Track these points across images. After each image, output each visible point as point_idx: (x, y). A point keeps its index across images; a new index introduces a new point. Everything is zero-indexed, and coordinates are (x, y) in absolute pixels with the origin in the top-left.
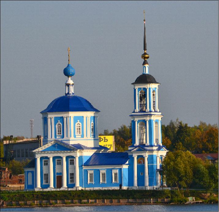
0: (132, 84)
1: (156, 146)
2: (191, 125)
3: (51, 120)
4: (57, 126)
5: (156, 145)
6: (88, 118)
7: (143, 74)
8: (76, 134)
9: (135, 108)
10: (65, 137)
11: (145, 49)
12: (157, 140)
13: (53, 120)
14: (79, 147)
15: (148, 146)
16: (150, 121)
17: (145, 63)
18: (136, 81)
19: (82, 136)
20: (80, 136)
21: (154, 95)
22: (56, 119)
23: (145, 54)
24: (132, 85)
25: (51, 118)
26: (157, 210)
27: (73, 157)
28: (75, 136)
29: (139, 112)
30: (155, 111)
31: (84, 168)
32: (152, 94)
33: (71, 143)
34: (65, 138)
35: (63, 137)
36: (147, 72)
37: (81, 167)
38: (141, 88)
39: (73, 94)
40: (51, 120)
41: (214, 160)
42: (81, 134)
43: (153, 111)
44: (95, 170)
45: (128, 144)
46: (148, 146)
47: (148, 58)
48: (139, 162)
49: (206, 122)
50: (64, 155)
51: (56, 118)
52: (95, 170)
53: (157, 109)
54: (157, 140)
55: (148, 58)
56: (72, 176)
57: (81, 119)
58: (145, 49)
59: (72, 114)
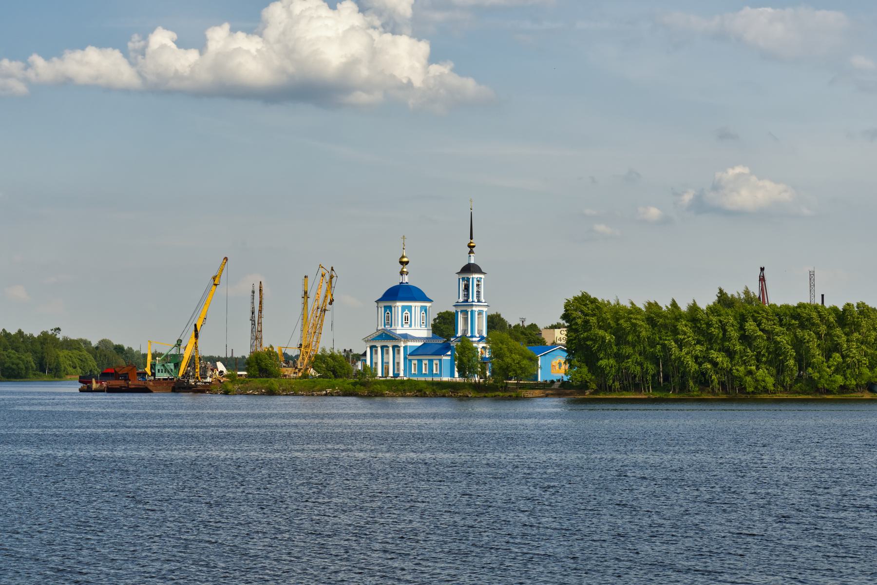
4: (386, 315)
5: (478, 335)
8: (404, 323)
11: (471, 238)
12: (480, 332)
14: (406, 337)
16: (472, 311)
17: (471, 252)
19: (411, 326)
22: (404, 308)
23: (471, 243)
24: (457, 275)
26: (46, 379)
27: (387, 347)
28: (402, 326)
30: (479, 301)
31: (410, 358)
33: (398, 332)
34: (393, 327)
35: (391, 326)
36: (472, 262)
37: (405, 358)
39: (407, 283)
42: (409, 323)
43: (476, 301)
44: (429, 360)
47: (474, 246)
49: (836, 305)
50: (390, 344)
51: (385, 307)
52: (429, 360)
53: (482, 299)
54: (480, 332)
55: (474, 246)
56: (396, 364)
57: (410, 308)
58: (471, 238)
59: (400, 304)
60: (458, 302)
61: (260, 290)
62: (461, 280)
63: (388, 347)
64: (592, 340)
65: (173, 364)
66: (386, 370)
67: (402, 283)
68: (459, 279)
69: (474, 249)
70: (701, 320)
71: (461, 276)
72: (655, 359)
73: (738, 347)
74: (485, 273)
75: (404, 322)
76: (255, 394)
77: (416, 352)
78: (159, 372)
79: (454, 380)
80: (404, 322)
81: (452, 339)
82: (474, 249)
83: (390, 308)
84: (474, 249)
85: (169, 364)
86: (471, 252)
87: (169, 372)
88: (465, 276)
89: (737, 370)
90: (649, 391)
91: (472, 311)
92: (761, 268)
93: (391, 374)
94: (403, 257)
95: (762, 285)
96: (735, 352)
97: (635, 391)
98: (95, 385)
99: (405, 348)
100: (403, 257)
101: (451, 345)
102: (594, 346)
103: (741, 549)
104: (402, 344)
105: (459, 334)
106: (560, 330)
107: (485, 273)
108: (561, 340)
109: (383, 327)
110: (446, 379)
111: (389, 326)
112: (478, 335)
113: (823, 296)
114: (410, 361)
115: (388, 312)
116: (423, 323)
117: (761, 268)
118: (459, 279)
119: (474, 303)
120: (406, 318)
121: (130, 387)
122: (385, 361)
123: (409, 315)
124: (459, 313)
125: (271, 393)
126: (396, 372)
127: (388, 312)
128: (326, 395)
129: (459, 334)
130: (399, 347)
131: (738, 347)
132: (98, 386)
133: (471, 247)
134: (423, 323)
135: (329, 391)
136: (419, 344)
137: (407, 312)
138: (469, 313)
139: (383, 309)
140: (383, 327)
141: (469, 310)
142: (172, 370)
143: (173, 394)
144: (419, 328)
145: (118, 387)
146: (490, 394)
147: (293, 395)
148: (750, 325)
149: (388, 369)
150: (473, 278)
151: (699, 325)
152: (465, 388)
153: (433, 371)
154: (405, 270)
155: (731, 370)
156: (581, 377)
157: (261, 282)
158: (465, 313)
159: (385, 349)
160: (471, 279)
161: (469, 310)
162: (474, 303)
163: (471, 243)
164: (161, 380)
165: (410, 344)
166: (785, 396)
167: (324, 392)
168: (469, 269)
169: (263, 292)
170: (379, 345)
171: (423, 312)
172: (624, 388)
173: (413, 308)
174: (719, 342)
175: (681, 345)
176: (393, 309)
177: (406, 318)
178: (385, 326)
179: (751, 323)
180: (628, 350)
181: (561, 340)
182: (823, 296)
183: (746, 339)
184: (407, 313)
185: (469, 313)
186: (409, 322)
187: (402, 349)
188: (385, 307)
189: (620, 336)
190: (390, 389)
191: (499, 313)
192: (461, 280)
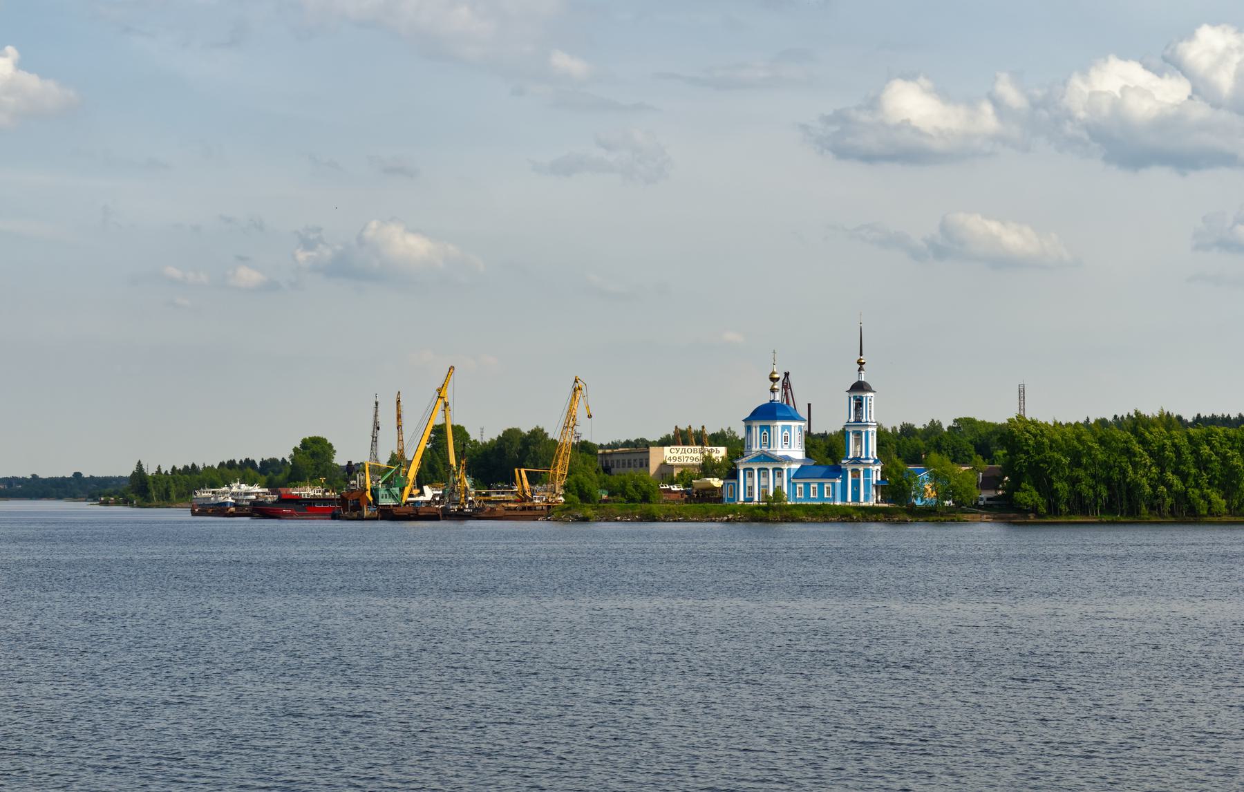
4: (762, 435)
5: (872, 458)
11: (861, 355)
16: (867, 433)
19: (790, 447)
28: (782, 447)
31: (793, 481)
33: (779, 454)
34: (772, 448)
35: (769, 447)
36: (863, 380)
37: (789, 481)
42: (768, 444)
44: (819, 484)
47: (864, 363)
50: (770, 467)
52: (819, 484)
55: (864, 363)
57: (789, 428)
58: (861, 355)
59: (780, 424)
62: (852, 398)
63: (753, 470)
64: (1046, 462)
65: (398, 489)
67: (773, 401)
68: (850, 398)
70: (1152, 443)
71: (852, 395)
72: (1108, 482)
73: (1193, 471)
74: (874, 392)
76: (628, 521)
77: (799, 474)
78: (382, 497)
79: (847, 504)
81: (843, 462)
82: (864, 366)
83: (768, 428)
85: (394, 489)
86: (860, 369)
87: (393, 497)
88: (858, 394)
89: (1193, 492)
90: (1097, 514)
92: (785, 373)
94: (774, 373)
95: (786, 394)
96: (1189, 474)
97: (1081, 514)
98: (366, 513)
99: (789, 470)
100: (774, 373)
101: (843, 467)
102: (1049, 469)
104: (785, 467)
105: (851, 456)
106: (669, 448)
107: (874, 392)
108: (671, 460)
109: (758, 449)
110: (838, 503)
111: (766, 447)
112: (872, 458)
113: (809, 405)
114: (795, 484)
115: (765, 432)
117: (785, 373)
118: (850, 398)
120: (786, 439)
121: (419, 514)
123: (789, 435)
124: (851, 433)
125: (650, 518)
127: (765, 432)
128: (728, 521)
129: (851, 456)
131: (1193, 471)
132: (369, 513)
135: (730, 516)
137: (786, 432)
138: (864, 433)
139: (758, 429)
140: (758, 449)
141: (863, 430)
142: (397, 495)
143: (332, 521)
145: (406, 514)
146: (931, 519)
147: (683, 521)
148: (1205, 450)
150: (866, 397)
151: (1150, 448)
152: (897, 513)
154: (776, 387)
155: (1186, 492)
156: (1033, 500)
158: (858, 434)
160: (865, 398)
161: (863, 430)
163: (861, 359)
164: (392, 507)
166: (1232, 519)
167: (726, 518)
168: (859, 387)
169: (401, 403)
170: (755, 467)
172: (1071, 512)
173: (793, 428)
174: (1172, 464)
175: (1135, 465)
176: (772, 429)
177: (786, 439)
178: (761, 446)
179: (1205, 446)
180: (1081, 473)
181: (671, 460)
182: (809, 405)
183: (1203, 464)
185: (864, 433)
186: (788, 442)
187: (785, 472)
188: (761, 427)
189: (1076, 462)
190: (808, 515)
191: (541, 427)
192: (852, 398)
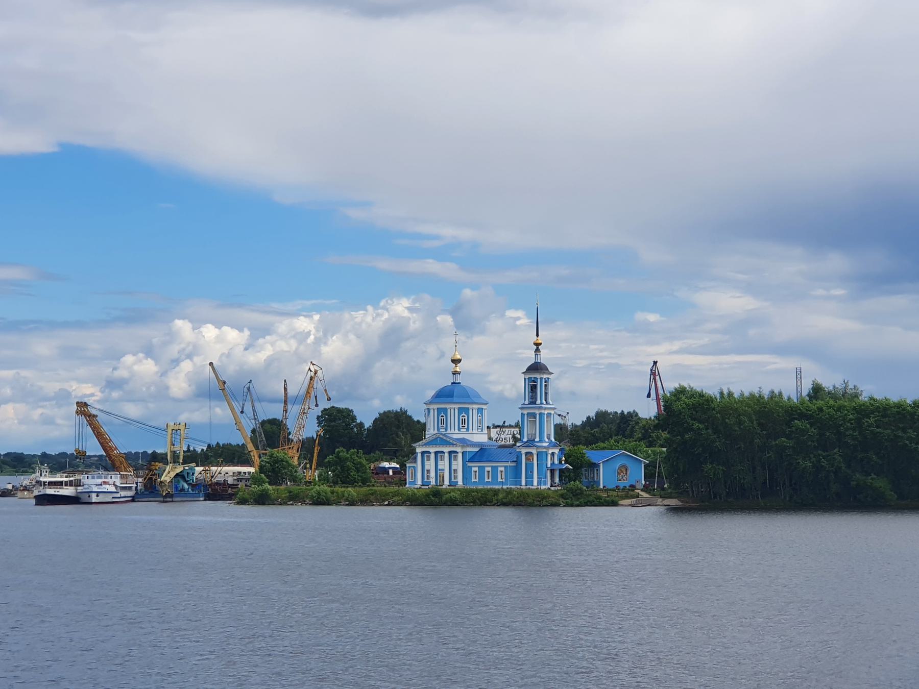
0: (522, 373)
1: (547, 442)
2: (640, 415)
3: (473, 411)
6: (474, 410)
7: (535, 362)
8: (461, 427)
9: (525, 400)
10: (484, 430)
11: (537, 335)
13: (436, 411)
14: (464, 442)
15: (537, 442)
18: (527, 370)
19: (468, 429)
20: (465, 430)
21: (546, 386)
24: (523, 374)
25: (454, 409)
28: (459, 429)
29: (529, 404)
31: (470, 464)
32: (544, 384)
33: (455, 436)
34: (449, 431)
35: (446, 430)
38: (531, 378)
40: (473, 411)
41: (127, 632)
42: (466, 427)
44: (492, 467)
45: (247, 480)
46: (537, 442)
47: (540, 344)
48: (527, 459)
50: (446, 450)
51: (459, 409)
52: (492, 467)
55: (540, 344)
58: (537, 335)
60: (524, 404)
61: (285, 388)
66: (117, 453)
69: (540, 347)
75: (461, 425)
80: (461, 425)
84: (540, 347)
88: (533, 376)
91: (540, 414)
92: (654, 362)
93: (447, 482)
103: (212, 598)
111: (444, 430)
115: (442, 414)
116: (480, 426)
117: (654, 362)
118: (525, 379)
119: (543, 406)
120: (463, 421)
122: (440, 467)
123: (466, 418)
126: (453, 480)
130: (458, 453)
133: (537, 345)
134: (480, 426)
136: (476, 449)
137: (464, 414)
140: (436, 432)
144: (477, 432)
149: (443, 477)
150: (541, 379)
153: (498, 479)
157: (285, 381)
159: (426, 455)
162: (543, 406)
165: (469, 449)
171: (479, 415)
177: (463, 421)
178: (438, 430)
184: (442, 416)
186: (466, 425)
